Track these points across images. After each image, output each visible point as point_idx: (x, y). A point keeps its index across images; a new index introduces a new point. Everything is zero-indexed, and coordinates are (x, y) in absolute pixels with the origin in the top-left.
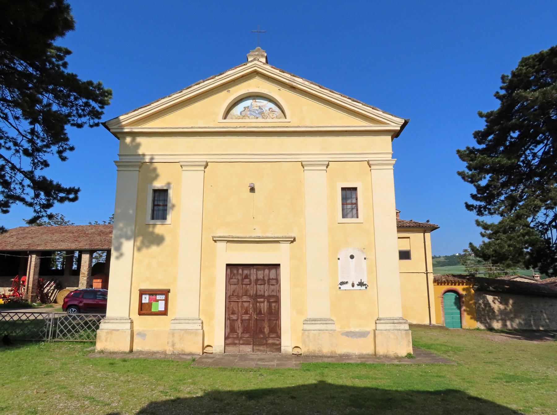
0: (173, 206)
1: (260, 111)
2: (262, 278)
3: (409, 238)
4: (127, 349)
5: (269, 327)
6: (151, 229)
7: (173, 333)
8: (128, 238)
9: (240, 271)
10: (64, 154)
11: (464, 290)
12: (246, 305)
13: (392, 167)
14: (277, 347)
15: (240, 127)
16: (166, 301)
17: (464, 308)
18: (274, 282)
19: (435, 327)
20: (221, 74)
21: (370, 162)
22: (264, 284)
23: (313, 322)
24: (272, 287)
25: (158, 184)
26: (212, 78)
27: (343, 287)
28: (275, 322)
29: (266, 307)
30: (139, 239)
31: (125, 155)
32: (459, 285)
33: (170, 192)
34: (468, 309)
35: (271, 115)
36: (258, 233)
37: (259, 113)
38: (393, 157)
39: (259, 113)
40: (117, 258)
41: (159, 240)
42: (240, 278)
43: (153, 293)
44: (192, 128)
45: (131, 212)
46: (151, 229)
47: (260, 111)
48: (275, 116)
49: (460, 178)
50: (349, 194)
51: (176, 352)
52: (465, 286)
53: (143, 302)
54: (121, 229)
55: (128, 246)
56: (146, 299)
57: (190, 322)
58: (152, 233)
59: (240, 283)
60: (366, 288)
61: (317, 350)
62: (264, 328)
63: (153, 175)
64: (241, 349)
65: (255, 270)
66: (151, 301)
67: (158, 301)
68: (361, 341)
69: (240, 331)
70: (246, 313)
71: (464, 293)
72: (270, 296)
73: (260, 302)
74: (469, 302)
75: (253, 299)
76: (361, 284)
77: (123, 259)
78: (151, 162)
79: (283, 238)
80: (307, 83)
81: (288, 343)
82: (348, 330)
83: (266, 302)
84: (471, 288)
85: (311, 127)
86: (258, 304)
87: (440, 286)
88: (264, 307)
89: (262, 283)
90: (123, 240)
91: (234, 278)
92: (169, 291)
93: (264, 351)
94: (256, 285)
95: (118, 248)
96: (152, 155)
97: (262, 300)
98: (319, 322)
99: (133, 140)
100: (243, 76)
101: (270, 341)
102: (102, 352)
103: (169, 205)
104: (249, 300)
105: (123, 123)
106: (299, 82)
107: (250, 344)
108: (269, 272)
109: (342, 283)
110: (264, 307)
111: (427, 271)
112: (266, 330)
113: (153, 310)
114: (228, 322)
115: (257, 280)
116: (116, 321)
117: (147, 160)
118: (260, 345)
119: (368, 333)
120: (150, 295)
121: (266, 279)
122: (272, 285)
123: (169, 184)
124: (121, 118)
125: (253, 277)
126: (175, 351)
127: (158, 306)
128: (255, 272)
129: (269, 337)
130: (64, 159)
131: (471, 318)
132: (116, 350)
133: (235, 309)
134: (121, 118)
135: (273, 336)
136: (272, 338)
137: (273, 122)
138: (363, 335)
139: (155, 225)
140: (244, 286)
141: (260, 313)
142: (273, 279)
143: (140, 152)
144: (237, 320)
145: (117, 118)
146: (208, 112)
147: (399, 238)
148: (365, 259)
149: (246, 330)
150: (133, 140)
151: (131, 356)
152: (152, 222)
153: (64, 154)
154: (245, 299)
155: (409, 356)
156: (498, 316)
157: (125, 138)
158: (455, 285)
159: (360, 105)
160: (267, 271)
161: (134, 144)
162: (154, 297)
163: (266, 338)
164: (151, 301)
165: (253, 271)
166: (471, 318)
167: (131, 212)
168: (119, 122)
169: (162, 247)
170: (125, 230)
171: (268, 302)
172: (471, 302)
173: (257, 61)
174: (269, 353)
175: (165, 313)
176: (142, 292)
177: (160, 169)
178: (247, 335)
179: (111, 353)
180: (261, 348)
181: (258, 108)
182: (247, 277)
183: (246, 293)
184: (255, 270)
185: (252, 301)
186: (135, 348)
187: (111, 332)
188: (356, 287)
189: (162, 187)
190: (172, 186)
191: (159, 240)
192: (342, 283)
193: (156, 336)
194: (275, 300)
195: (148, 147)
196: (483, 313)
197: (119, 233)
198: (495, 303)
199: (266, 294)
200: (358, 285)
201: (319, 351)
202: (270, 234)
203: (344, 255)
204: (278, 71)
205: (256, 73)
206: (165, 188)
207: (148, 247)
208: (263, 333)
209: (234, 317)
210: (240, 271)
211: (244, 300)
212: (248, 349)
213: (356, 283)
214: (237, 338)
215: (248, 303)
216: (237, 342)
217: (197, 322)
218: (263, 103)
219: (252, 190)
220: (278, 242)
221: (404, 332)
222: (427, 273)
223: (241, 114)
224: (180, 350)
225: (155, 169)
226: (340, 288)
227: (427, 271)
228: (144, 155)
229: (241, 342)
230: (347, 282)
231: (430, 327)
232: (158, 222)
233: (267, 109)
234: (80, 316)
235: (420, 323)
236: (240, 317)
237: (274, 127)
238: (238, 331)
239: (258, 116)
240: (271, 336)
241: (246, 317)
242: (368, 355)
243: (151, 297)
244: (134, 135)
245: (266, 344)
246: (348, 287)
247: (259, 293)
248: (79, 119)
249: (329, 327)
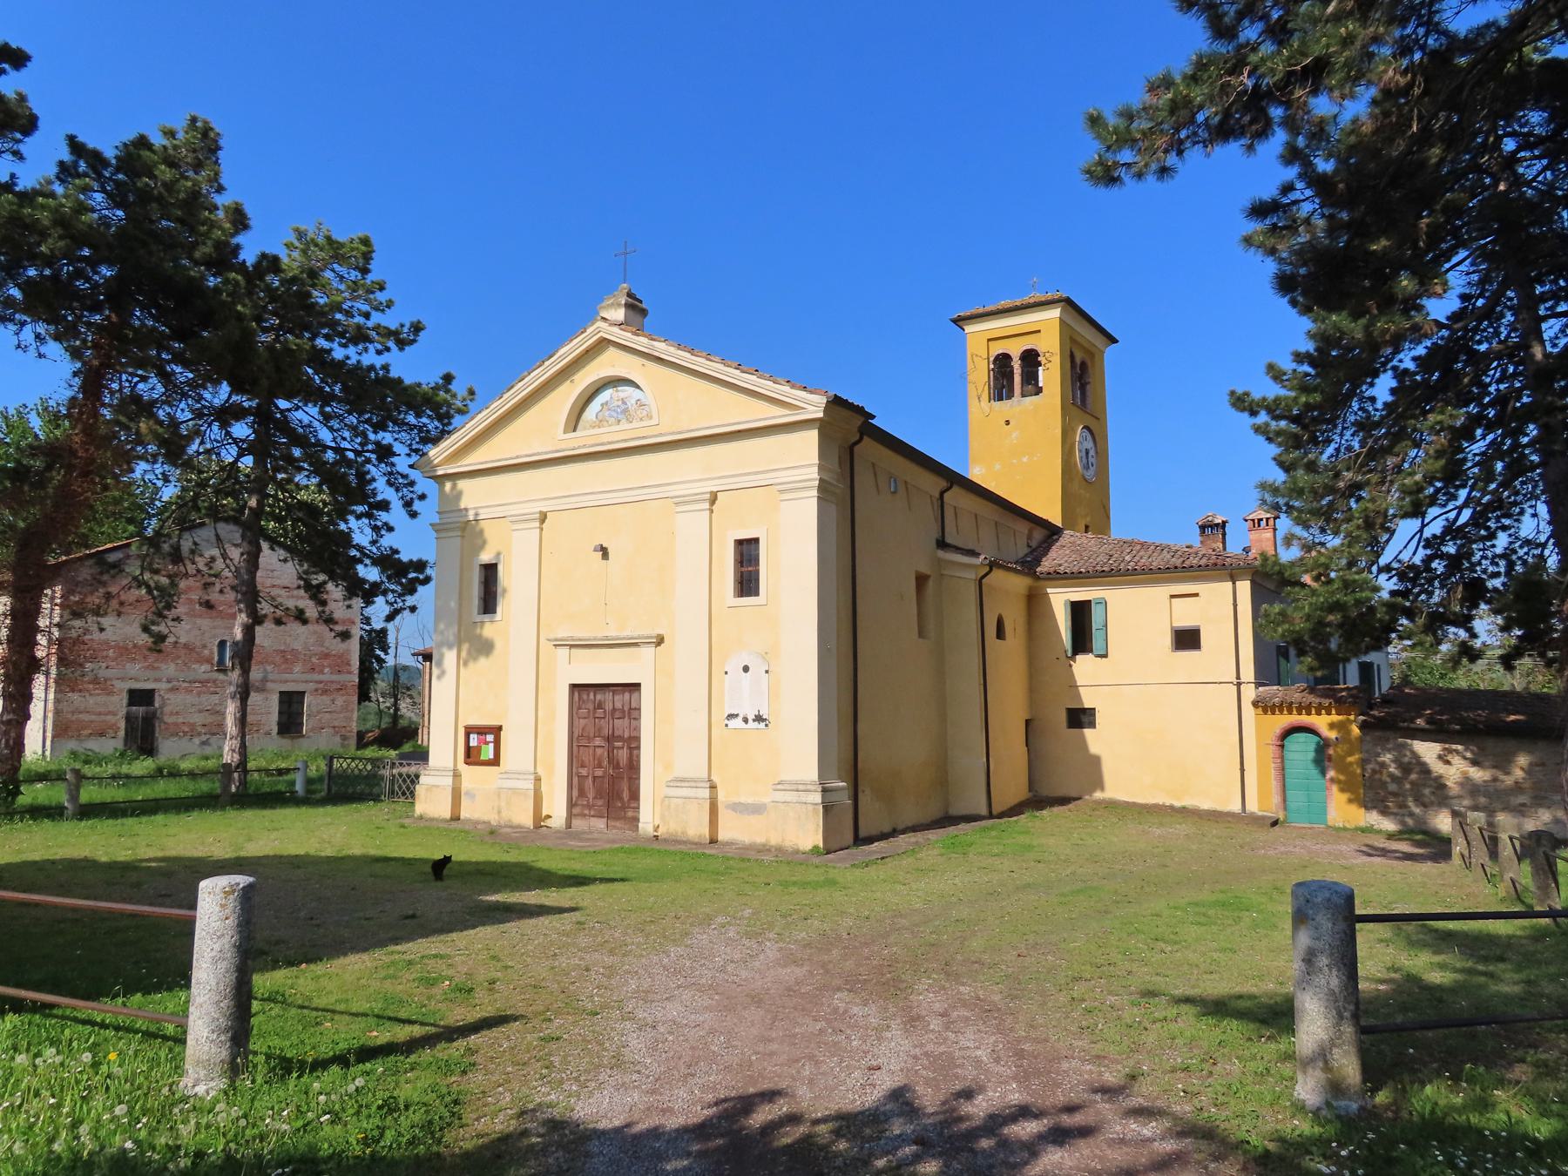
3: (1196, 595)
4: (447, 815)
7: (499, 792)
8: (450, 647)
11: (1332, 726)
12: (599, 751)
17: (1331, 774)
19: (1255, 820)
25: (486, 557)
27: (734, 723)
32: (1319, 714)
33: (500, 568)
34: (1342, 777)
36: (612, 632)
40: (439, 677)
41: (486, 648)
42: (591, 707)
43: (482, 731)
49: (1261, 439)
50: (747, 552)
52: (1335, 718)
56: (474, 740)
58: (480, 636)
66: (482, 742)
69: (591, 795)
70: (600, 766)
71: (1333, 735)
74: (1344, 758)
76: (759, 719)
81: (649, 817)
82: (736, 800)
84: (1351, 722)
87: (1269, 717)
90: (445, 650)
92: (500, 728)
100: (587, 351)
102: (421, 817)
109: (731, 716)
111: (1238, 677)
114: (575, 780)
118: (617, 819)
125: (609, 706)
131: (1350, 801)
141: (617, 766)
147: (1172, 596)
151: (454, 825)
154: (598, 742)
156: (1459, 797)
158: (1309, 714)
160: (627, 695)
166: (1350, 801)
169: (492, 658)
172: (1350, 759)
175: (495, 762)
176: (469, 731)
177: (490, 531)
178: (600, 802)
179: (432, 819)
180: (618, 824)
183: (598, 734)
186: (464, 814)
187: (431, 788)
188: (752, 724)
191: (486, 648)
192: (731, 716)
196: (1392, 787)
198: (1448, 763)
205: (603, 344)
207: (475, 659)
208: (621, 799)
209: (584, 772)
212: (600, 824)
213: (751, 717)
214: (589, 807)
220: (636, 645)
222: (1239, 685)
227: (1238, 677)
231: (1244, 819)
235: (1219, 808)
242: (797, 852)
246: (737, 723)
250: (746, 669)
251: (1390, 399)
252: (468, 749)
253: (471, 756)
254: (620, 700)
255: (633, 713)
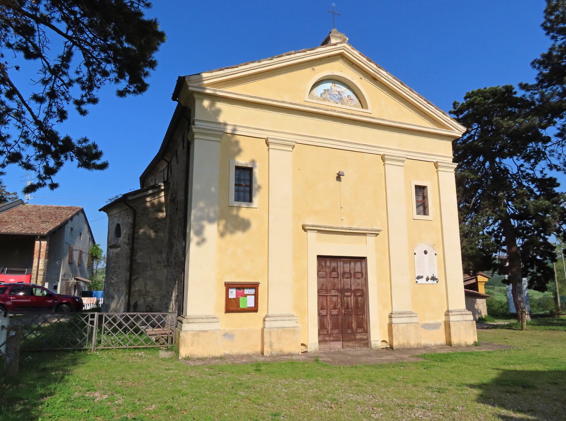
0: (259, 187)
1: (339, 96)
2: (348, 271)
5: (357, 321)
6: (235, 212)
8: (211, 221)
9: (328, 263)
10: (84, 107)
12: (334, 299)
13: (453, 170)
14: (366, 342)
15: (331, 110)
16: (256, 295)
18: (359, 275)
20: (312, 50)
21: (439, 164)
22: (351, 278)
23: (400, 316)
24: (359, 281)
25: (242, 161)
26: (304, 52)
27: (420, 281)
28: (361, 316)
29: (352, 301)
30: (223, 222)
31: (203, 121)
33: (257, 172)
35: (349, 102)
37: (339, 99)
38: (454, 161)
39: (339, 99)
40: (199, 244)
41: (244, 225)
42: (328, 271)
43: (240, 287)
44: (283, 102)
45: (213, 189)
46: (235, 212)
47: (339, 96)
48: (353, 104)
50: (421, 190)
51: (274, 353)
53: (230, 297)
54: (202, 210)
55: (211, 230)
56: (233, 294)
57: (286, 318)
58: (237, 216)
59: (328, 276)
60: (437, 282)
61: (406, 342)
62: (352, 323)
63: (236, 149)
64: (332, 346)
65: (342, 263)
66: (239, 296)
67: (246, 296)
68: (434, 332)
69: (329, 327)
70: (335, 308)
72: (356, 290)
73: (347, 296)
75: (343, 293)
76: (433, 278)
77: (205, 246)
78: (233, 134)
79: (371, 230)
80: (390, 77)
81: (377, 336)
83: (352, 296)
85: (394, 122)
86: (345, 298)
88: (351, 301)
89: (349, 276)
91: (322, 270)
93: (353, 347)
94: (343, 278)
95: (199, 232)
96: (235, 126)
97: (349, 294)
98: (405, 315)
99: (212, 105)
101: (358, 336)
102: (187, 359)
103: (255, 186)
104: (337, 294)
105: (206, 82)
106: (384, 75)
107: (340, 341)
108: (355, 265)
109: (419, 278)
110: (351, 301)
112: (354, 325)
113: (242, 306)
115: (344, 273)
116: (202, 321)
117: (229, 131)
118: (349, 341)
119: (440, 324)
120: (237, 288)
121: (352, 272)
122: (358, 278)
123: (253, 162)
124: (204, 75)
126: (273, 353)
127: (246, 301)
128: (342, 265)
129: (357, 333)
130: (83, 113)
132: (205, 356)
133: (325, 304)
134: (204, 75)
135: (361, 331)
136: (359, 333)
137: (352, 108)
138: (435, 326)
139: (239, 207)
140: (332, 279)
141: (347, 308)
142: (358, 272)
143: (221, 119)
144: (326, 316)
145: (199, 74)
146: (294, 87)
148: (436, 254)
149: (335, 326)
150: (212, 105)
152: (237, 204)
153: (84, 107)
154: (333, 293)
155: (476, 344)
157: (202, 100)
159: (434, 108)
160: (353, 264)
161: (213, 109)
162: (241, 291)
163: (354, 333)
164: (239, 296)
165: (340, 264)
167: (213, 189)
168: (201, 80)
170: (206, 210)
171: (355, 296)
173: (339, 44)
174: (358, 348)
175: (255, 309)
176: (229, 286)
177: (244, 143)
178: (336, 331)
180: (350, 344)
181: (337, 93)
182: (334, 270)
184: (342, 263)
185: (339, 295)
187: (197, 333)
188: (430, 282)
189: (246, 164)
190: (258, 164)
191: (244, 225)
192: (419, 278)
193: (237, 337)
194: (362, 294)
195: (229, 115)
197: (199, 214)
199: (353, 288)
200: (431, 279)
201: (408, 344)
202: (356, 226)
203: (419, 250)
204: (365, 59)
205: (341, 56)
206: (250, 166)
207: (232, 232)
210: (328, 263)
211: (333, 294)
212: (338, 345)
213: (430, 277)
215: (336, 298)
216: (327, 338)
217: (292, 318)
218: (343, 89)
219: (339, 178)
220: (365, 234)
221: (470, 322)
223: (321, 96)
224: (278, 350)
225: (237, 143)
226: (417, 282)
228: (225, 124)
229: (331, 339)
230: (422, 277)
232: (244, 204)
233: (346, 95)
234: (134, 315)
236: (329, 312)
237: (362, 116)
238: (328, 328)
239: (338, 101)
240: (358, 331)
241: (335, 312)
242: (441, 345)
243: (238, 291)
244: (214, 98)
245: (355, 340)
246: (423, 281)
247: (346, 287)
248: (108, 65)
249: (414, 320)
250: (426, 252)
251: (62, 136)
252: (228, 300)
253: (232, 307)
254: (358, 266)
255: (364, 274)
